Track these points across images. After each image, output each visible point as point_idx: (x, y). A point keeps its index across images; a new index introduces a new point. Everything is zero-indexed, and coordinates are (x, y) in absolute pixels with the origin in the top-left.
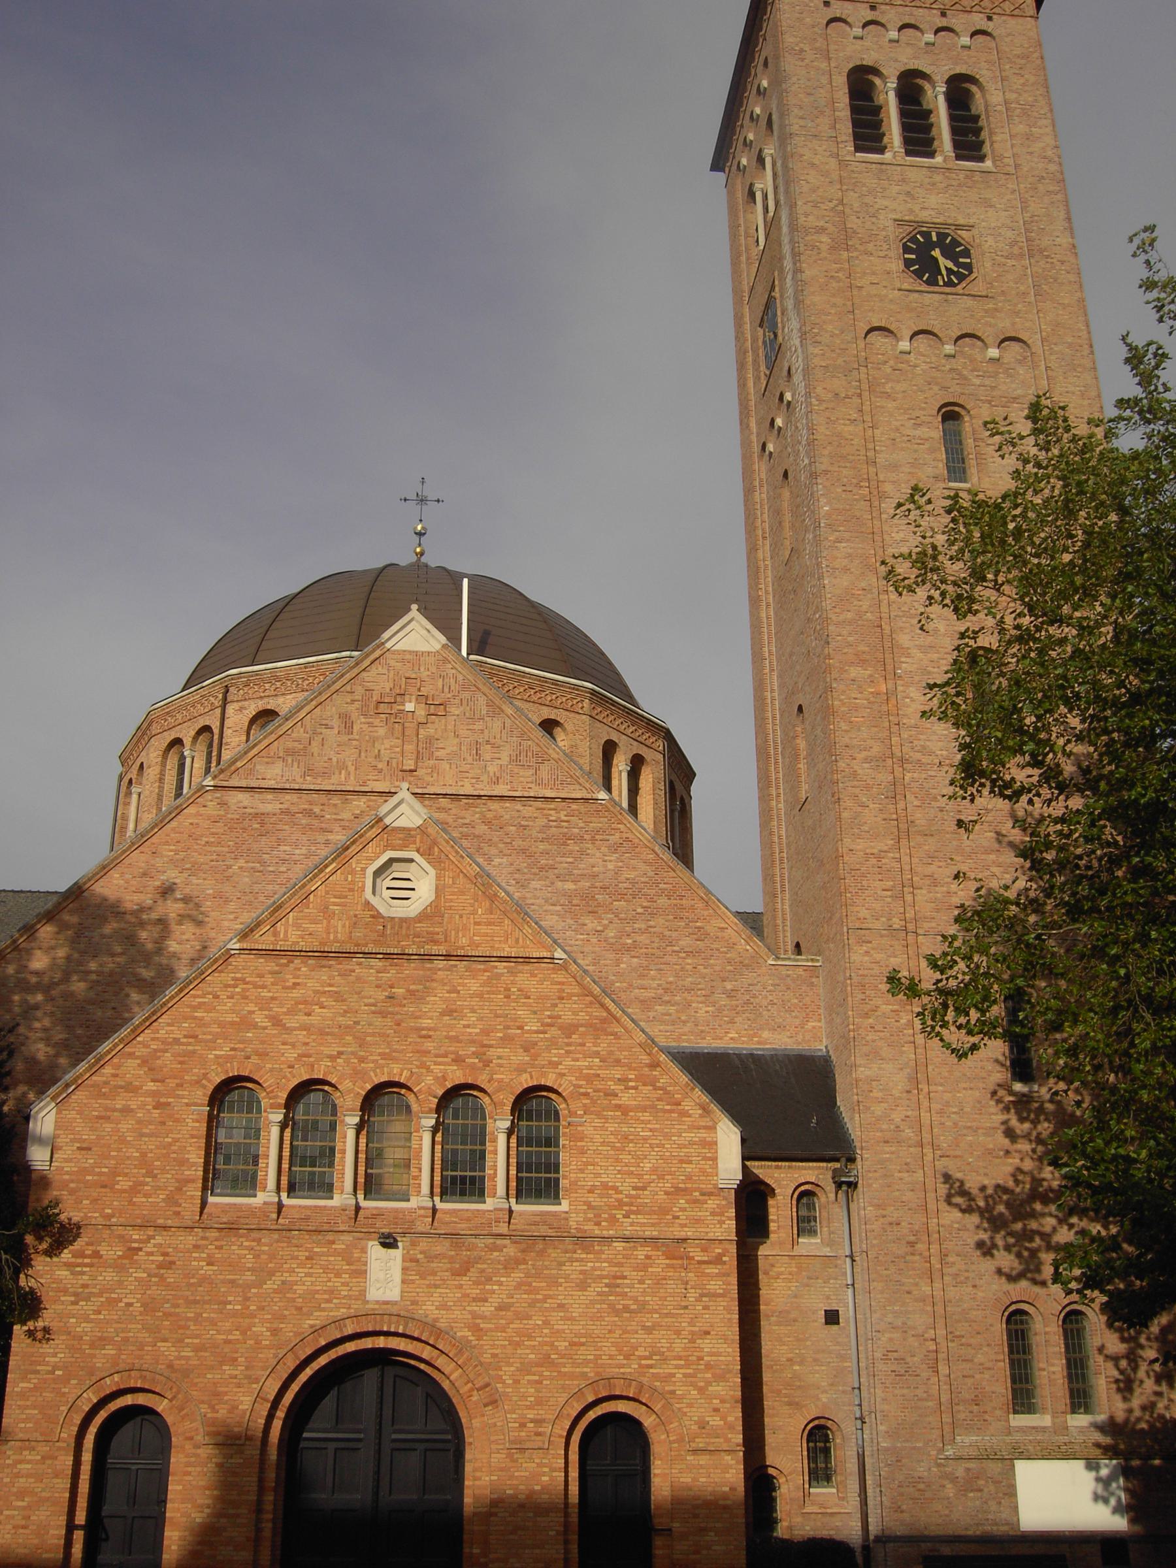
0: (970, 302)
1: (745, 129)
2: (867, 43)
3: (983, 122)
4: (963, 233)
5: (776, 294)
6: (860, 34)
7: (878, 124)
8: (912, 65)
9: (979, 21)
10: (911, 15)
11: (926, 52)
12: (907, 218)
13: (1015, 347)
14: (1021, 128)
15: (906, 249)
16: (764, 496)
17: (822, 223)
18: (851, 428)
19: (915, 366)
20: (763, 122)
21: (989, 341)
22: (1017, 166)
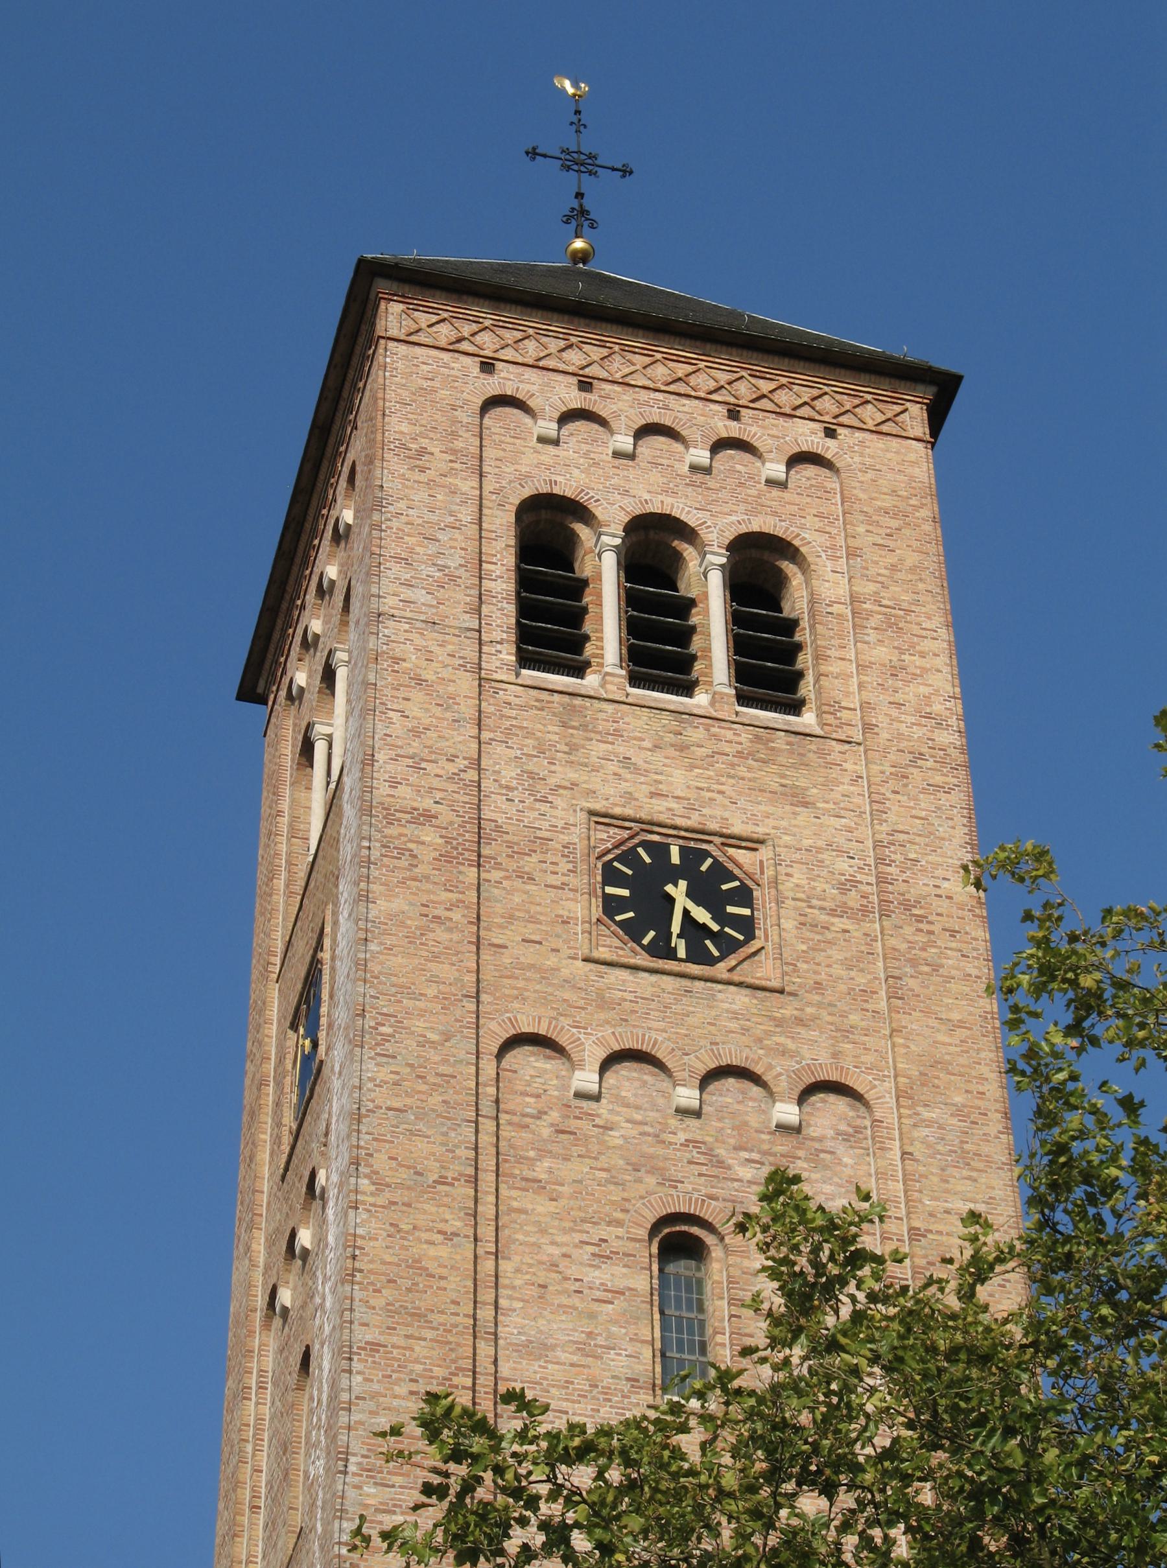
0: (740, 999)
1: (307, 613)
2: (567, 451)
3: (802, 635)
4: (741, 855)
5: (325, 955)
6: (553, 434)
7: (577, 617)
8: (660, 506)
9: (809, 437)
10: (666, 408)
11: (692, 484)
12: (617, 811)
13: (838, 1104)
14: (882, 653)
15: (611, 876)
16: (266, 1411)
17: (427, 803)
18: (443, 1252)
19: (607, 1128)
20: (338, 598)
21: (781, 1085)
22: (868, 727)
